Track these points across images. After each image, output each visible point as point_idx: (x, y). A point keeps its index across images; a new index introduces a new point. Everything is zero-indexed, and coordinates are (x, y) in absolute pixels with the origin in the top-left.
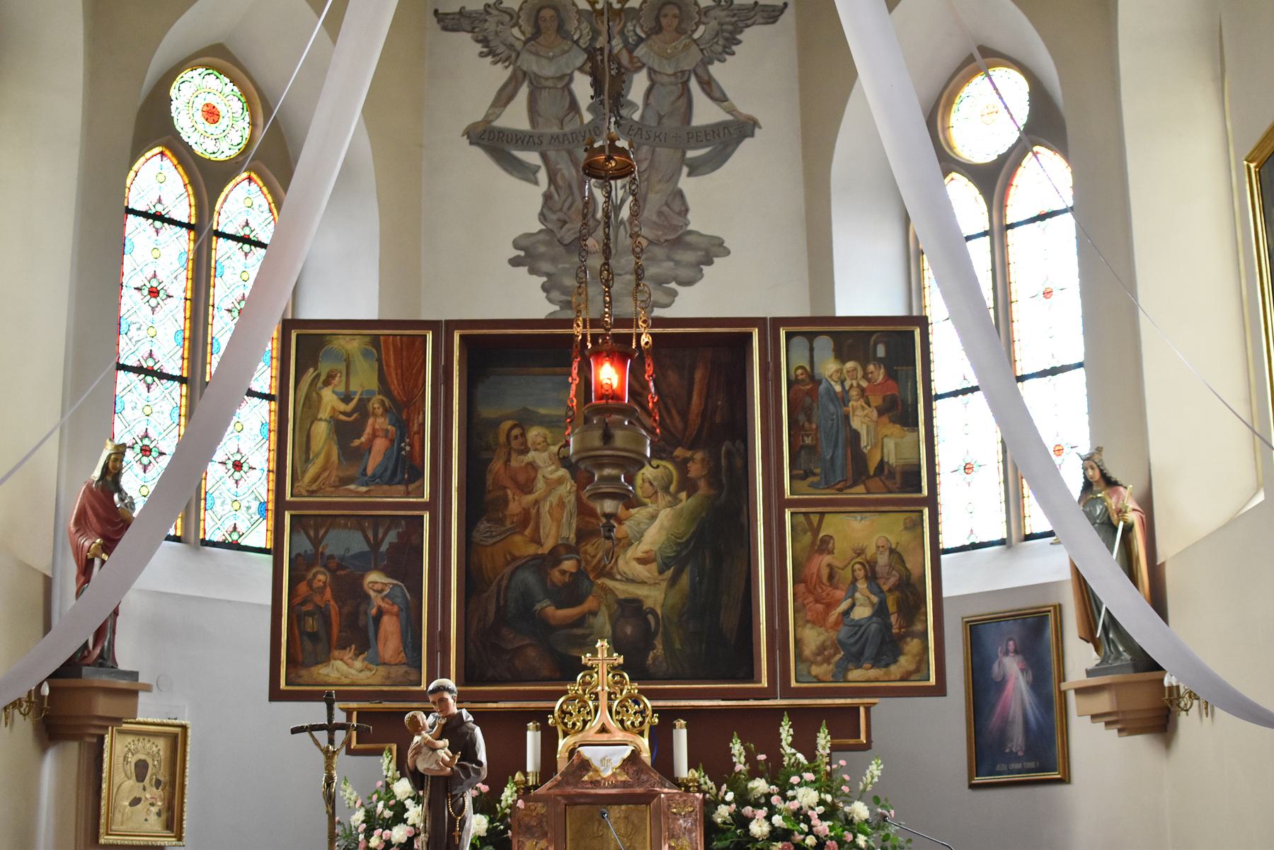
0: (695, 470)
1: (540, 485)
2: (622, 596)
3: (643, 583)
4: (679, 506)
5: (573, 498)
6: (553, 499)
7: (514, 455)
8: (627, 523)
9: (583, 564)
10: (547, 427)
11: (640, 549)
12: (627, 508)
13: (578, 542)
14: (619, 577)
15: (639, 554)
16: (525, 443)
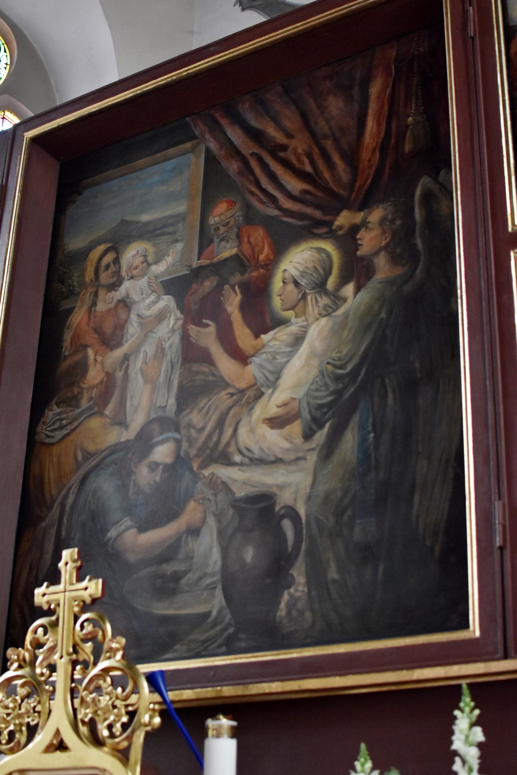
0: (368, 241)
1: (133, 329)
2: (240, 493)
3: (278, 461)
4: (341, 311)
5: (176, 339)
6: (149, 348)
7: (102, 293)
8: (256, 360)
9: (185, 445)
10: (149, 240)
11: (272, 404)
12: (257, 336)
13: (180, 409)
14: (237, 458)
15: (273, 410)
16: (117, 273)
